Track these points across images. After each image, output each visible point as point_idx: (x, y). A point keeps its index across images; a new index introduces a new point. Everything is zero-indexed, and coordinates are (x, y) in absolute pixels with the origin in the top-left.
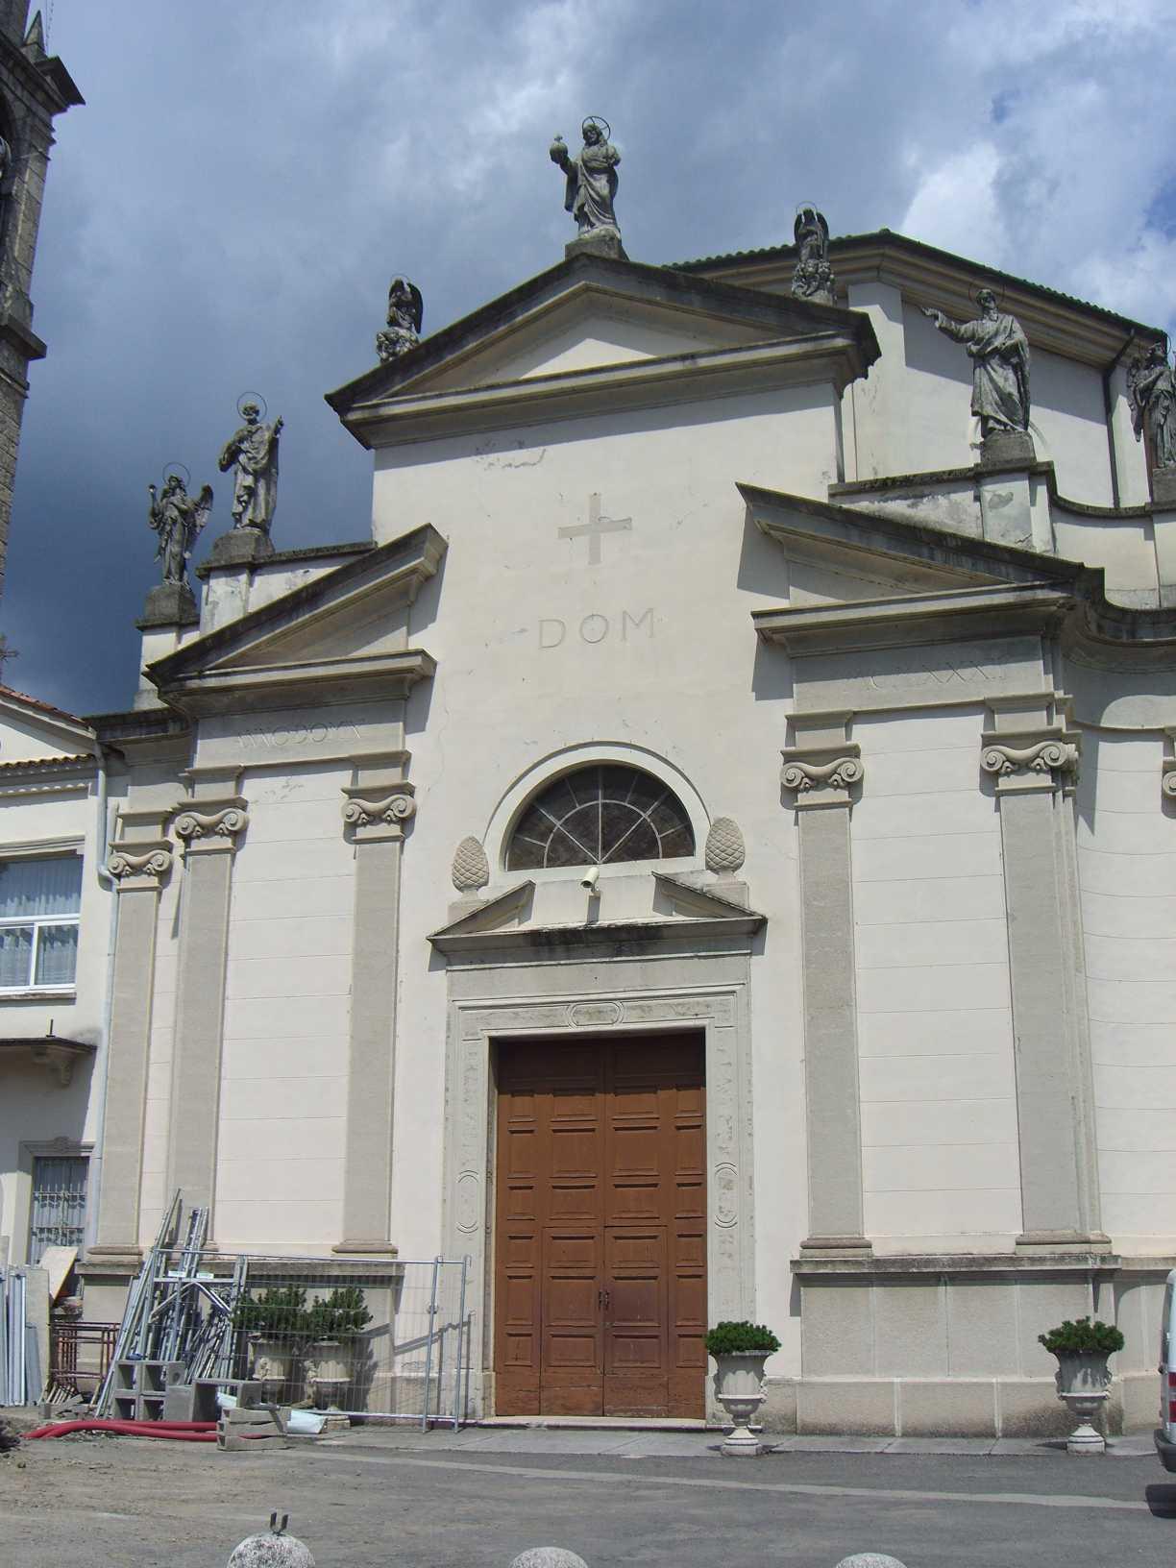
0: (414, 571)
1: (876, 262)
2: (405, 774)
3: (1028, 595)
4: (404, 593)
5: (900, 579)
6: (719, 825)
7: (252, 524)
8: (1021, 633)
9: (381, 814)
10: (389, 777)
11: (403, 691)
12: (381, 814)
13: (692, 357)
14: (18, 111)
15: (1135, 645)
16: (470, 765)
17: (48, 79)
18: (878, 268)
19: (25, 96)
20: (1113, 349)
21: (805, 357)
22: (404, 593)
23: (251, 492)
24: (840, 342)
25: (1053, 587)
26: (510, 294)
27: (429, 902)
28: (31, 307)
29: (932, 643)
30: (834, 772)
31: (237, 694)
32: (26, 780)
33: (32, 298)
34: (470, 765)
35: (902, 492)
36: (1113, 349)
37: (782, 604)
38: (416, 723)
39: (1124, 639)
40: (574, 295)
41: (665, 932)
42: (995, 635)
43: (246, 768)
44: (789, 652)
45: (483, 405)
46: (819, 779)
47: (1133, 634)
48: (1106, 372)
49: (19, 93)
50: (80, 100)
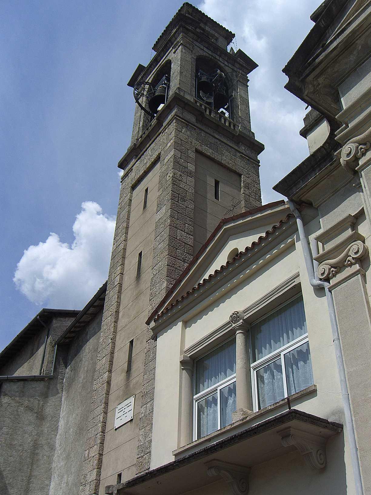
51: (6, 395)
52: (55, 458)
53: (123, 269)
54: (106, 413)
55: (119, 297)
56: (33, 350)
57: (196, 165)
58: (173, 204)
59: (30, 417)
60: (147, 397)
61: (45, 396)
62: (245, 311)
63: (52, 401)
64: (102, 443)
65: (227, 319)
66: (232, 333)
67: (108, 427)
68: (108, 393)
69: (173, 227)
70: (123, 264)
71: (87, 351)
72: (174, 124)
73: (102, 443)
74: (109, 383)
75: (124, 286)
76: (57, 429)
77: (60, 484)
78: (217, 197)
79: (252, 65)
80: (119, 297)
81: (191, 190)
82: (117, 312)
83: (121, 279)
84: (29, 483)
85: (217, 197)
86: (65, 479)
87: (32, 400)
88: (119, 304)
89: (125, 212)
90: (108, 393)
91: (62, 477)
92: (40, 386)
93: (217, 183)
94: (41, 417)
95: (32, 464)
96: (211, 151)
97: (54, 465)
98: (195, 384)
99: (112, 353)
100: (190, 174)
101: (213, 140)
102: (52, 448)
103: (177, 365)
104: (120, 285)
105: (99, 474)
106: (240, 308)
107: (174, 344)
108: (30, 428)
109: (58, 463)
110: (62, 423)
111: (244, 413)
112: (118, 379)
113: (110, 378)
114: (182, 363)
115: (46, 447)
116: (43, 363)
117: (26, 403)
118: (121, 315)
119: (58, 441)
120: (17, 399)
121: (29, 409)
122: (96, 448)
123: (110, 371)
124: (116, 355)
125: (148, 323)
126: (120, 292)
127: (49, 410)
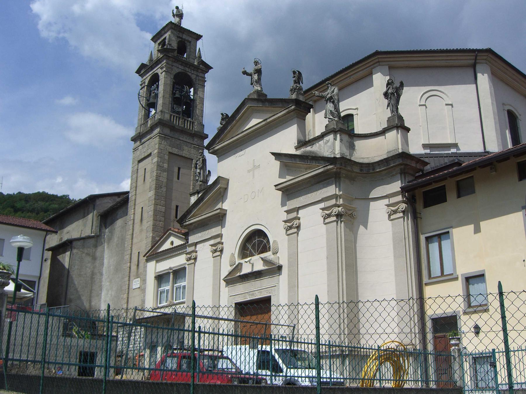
0: (220, 188)
1: (377, 60)
2: (221, 239)
3: (326, 168)
4: (220, 193)
5: (306, 169)
6: (274, 241)
7: (200, 181)
8: (330, 178)
9: (218, 251)
10: (218, 240)
11: (220, 218)
12: (218, 251)
13: (266, 119)
14: (193, 77)
15: (374, 173)
16: (233, 234)
17: (201, 66)
18: (379, 62)
19: (195, 73)
20: (473, 59)
21: (288, 113)
22: (220, 193)
23: (200, 173)
24: (293, 107)
25: (331, 164)
26: (274, 99)
27: (226, 269)
28: (204, 126)
29: (312, 185)
30: (398, 208)
31: (194, 225)
32: (169, 253)
33: (204, 123)
34: (233, 234)
35: (309, 144)
36: (473, 59)
37: (285, 180)
38: (223, 226)
39: (371, 171)
40: (247, 109)
41: (262, 272)
42: (325, 180)
43: (197, 242)
44: (288, 192)
45: (237, 140)
46: (293, 226)
47: (374, 169)
48: (474, 66)
49: (193, 72)
50: (211, 68)
51: (75, 248)
52: (104, 279)
53: (134, 211)
54: (129, 281)
55: (133, 227)
56: (84, 213)
57: (168, 164)
58: (156, 191)
59: (89, 259)
60: (144, 281)
61: (96, 246)
62: (174, 267)
63: (99, 249)
64: (128, 293)
65: (168, 268)
66: (168, 273)
67: (130, 288)
68: (130, 272)
69: (156, 204)
70: (135, 209)
71: (118, 225)
72: (157, 140)
73: (128, 293)
74: (130, 268)
75: (136, 221)
76: (103, 264)
77: (107, 294)
78: (178, 179)
79: (208, 68)
80: (133, 227)
81: (165, 181)
82: (133, 234)
83: (134, 217)
84: (91, 293)
85: (178, 179)
86: (110, 293)
87: (89, 249)
88: (133, 229)
89: (135, 176)
90: (130, 272)
91: (108, 291)
92: (92, 241)
93: (179, 169)
94: (94, 258)
95: (92, 283)
96: (177, 150)
97: (103, 283)
98: (159, 284)
99: (131, 254)
100: (164, 171)
101: (178, 142)
102: (102, 274)
103: (153, 278)
104: (134, 220)
105: (127, 305)
106: (172, 266)
107: (153, 268)
108: (89, 265)
109: (106, 283)
110: (106, 261)
111: (171, 302)
112: (134, 268)
113: (130, 265)
114: (155, 277)
115: (98, 274)
116: (92, 226)
117: (86, 251)
118: (134, 236)
119: (105, 270)
120: (81, 250)
121: (88, 254)
122: (127, 286)
123: (130, 262)
124: (133, 255)
125: (144, 256)
126: (133, 223)
127: (98, 254)
